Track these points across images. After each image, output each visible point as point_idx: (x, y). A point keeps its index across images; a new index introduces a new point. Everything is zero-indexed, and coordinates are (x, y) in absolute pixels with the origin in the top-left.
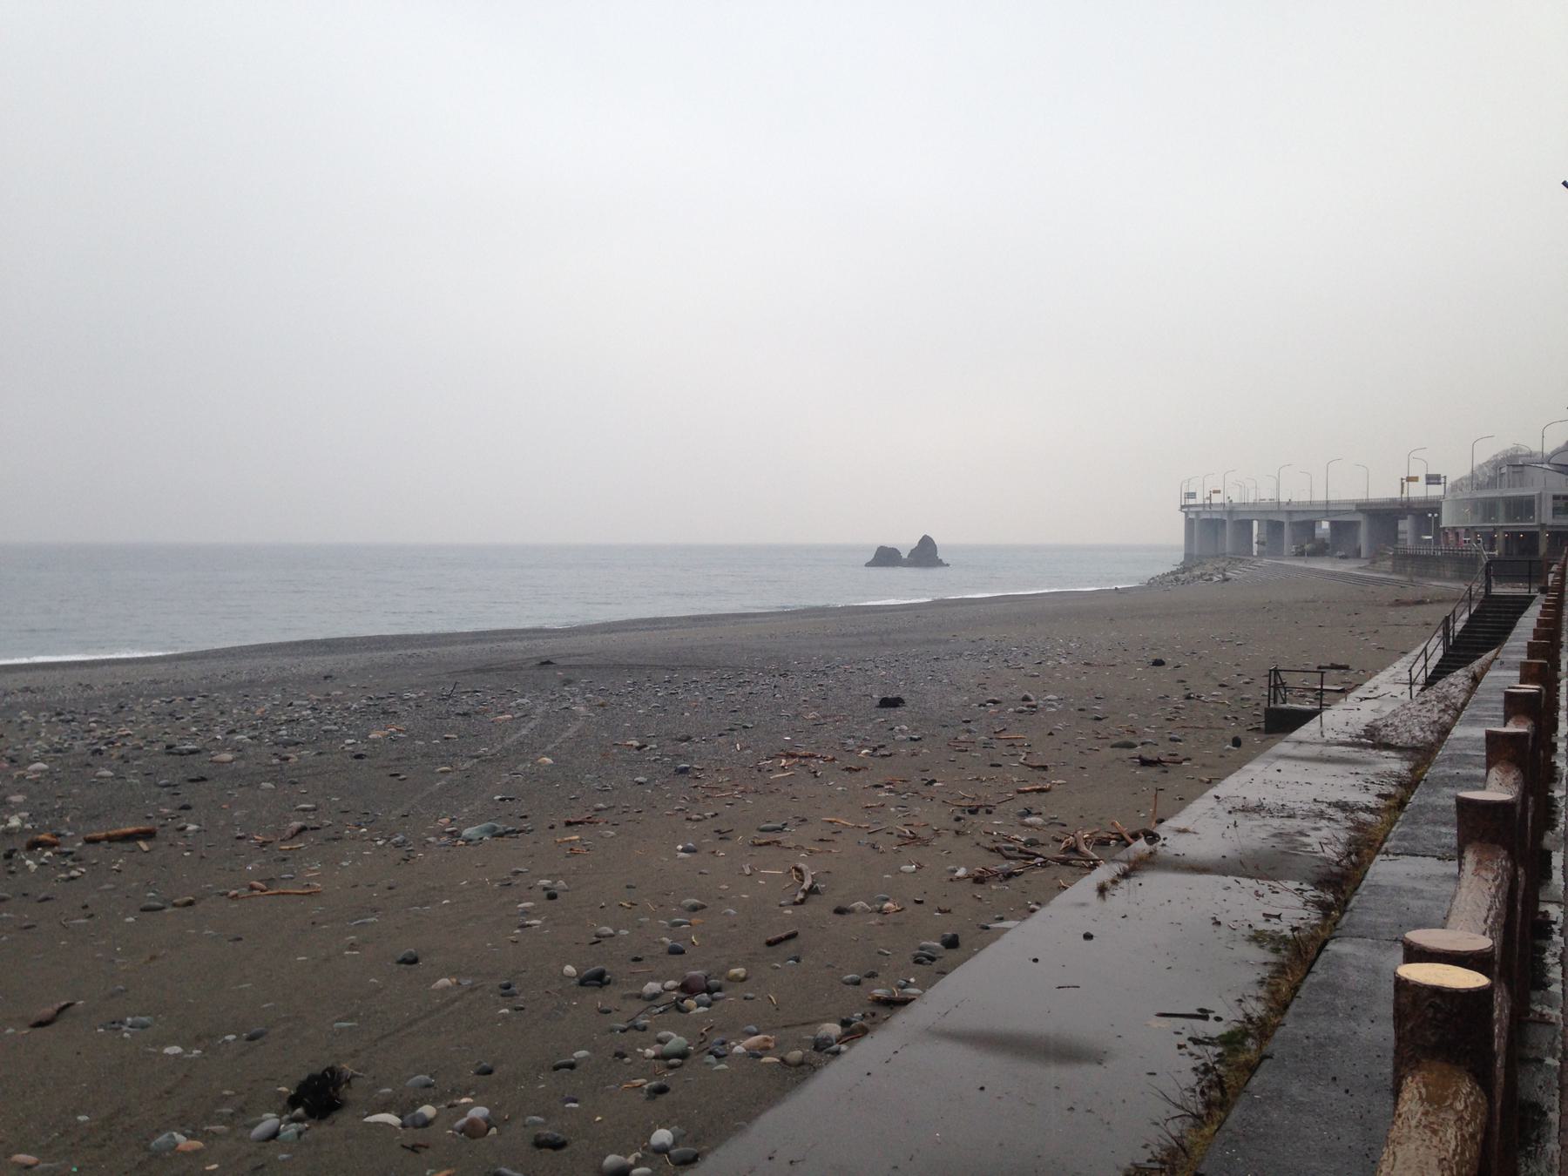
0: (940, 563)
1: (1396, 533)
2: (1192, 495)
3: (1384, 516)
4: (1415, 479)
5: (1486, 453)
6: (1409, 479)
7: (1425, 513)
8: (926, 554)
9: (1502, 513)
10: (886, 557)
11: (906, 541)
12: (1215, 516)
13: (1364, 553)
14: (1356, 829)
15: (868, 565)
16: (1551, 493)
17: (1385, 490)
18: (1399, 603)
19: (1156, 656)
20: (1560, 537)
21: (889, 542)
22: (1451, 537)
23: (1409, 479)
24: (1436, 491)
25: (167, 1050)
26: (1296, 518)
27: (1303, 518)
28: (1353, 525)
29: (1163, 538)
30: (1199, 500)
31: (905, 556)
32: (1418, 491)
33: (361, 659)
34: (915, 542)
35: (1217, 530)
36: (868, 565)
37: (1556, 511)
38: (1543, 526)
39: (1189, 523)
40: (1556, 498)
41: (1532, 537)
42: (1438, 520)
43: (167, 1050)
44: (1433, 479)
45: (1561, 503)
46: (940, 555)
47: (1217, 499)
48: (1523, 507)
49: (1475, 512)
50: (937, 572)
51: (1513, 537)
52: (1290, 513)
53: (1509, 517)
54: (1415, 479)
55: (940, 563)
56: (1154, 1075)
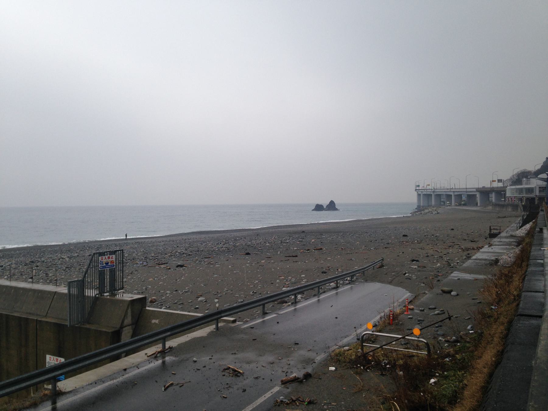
0: (336, 209)
1: (489, 197)
2: (419, 186)
3: (485, 193)
4: (495, 181)
5: (516, 172)
6: (493, 181)
7: (500, 192)
8: (332, 206)
9: (524, 192)
10: (319, 208)
11: (325, 202)
13: (479, 205)
14: (519, 244)
15: (313, 210)
17: (486, 184)
18: (499, 217)
19: (452, 227)
20: (541, 199)
21: (320, 203)
22: (510, 199)
23: (493, 181)
24: (500, 185)
26: (456, 194)
27: (458, 193)
28: (474, 196)
29: (412, 199)
30: (420, 188)
31: (325, 207)
32: (496, 185)
33: (180, 238)
34: (328, 203)
36: (313, 210)
37: (540, 191)
39: (419, 195)
40: (540, 188)
41: (533, 199)
42: (505, 194)
44: (500, 181)
45: (541, 189)
46: (336, 207)
49: (516, 192)
51: (527, 199)
52: (454, 192)
54: (495, 181)
55: (336, 209)
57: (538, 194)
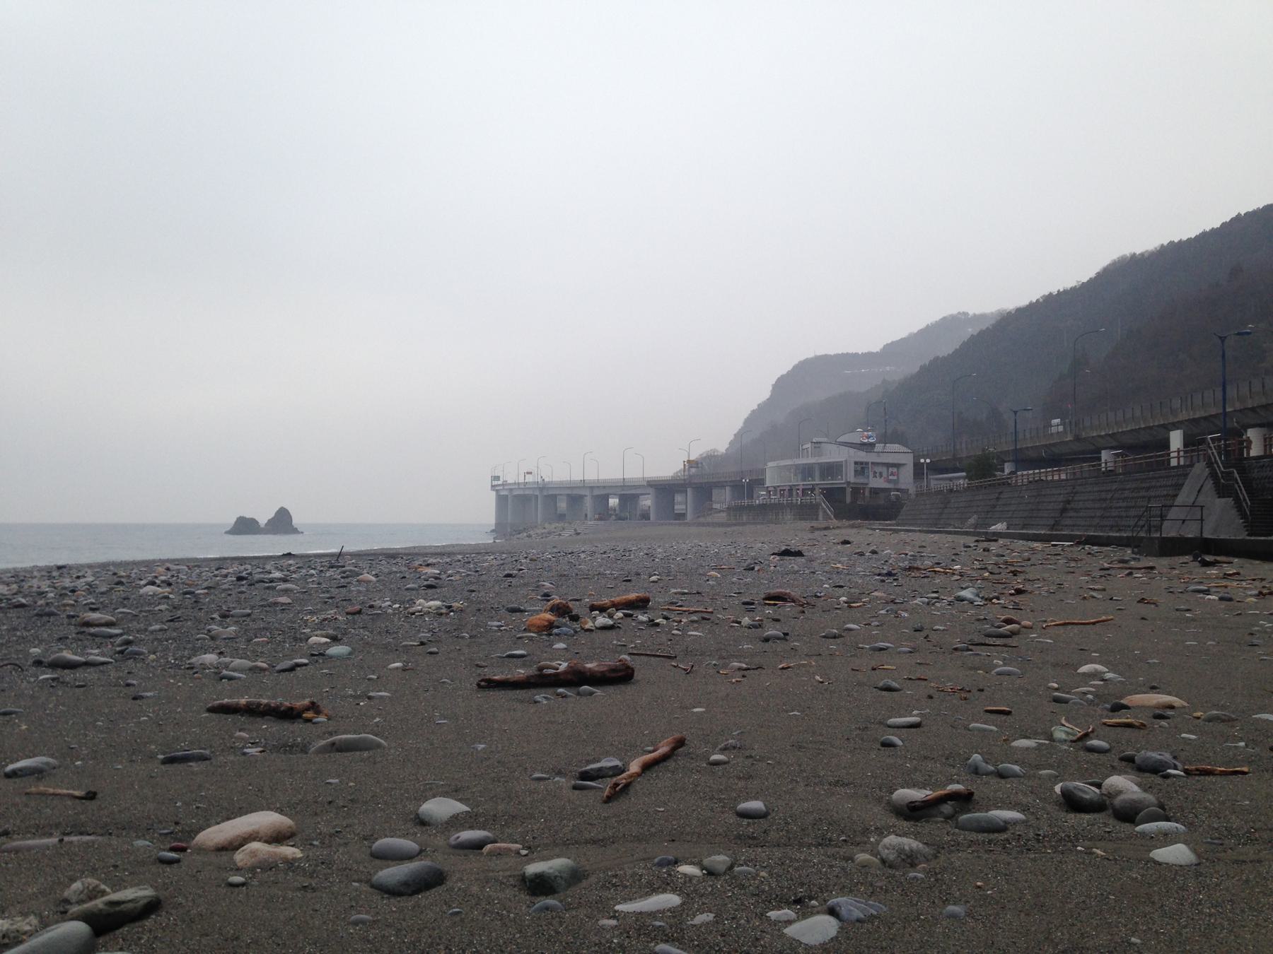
0: (295, 531)
2: (497, 478)
8: (282, 523)
9: (817, 474)
10: (245, 526)
12: (527, 492)
16: (853, 460)
25: (1139, 941)
26: (597, 492)
35: (522, 503)
38: (848, 483)
39: (502, 501)
40: (856, 463)
43: (1139, 941)
46: (295, 522)
47: (530, 479)
48: (831, 470)
50: (299, 537)
52: (592, 488)
53: (823, 477)
55: (295, 531)
56: (1264, 430)
57: (852, 479)
